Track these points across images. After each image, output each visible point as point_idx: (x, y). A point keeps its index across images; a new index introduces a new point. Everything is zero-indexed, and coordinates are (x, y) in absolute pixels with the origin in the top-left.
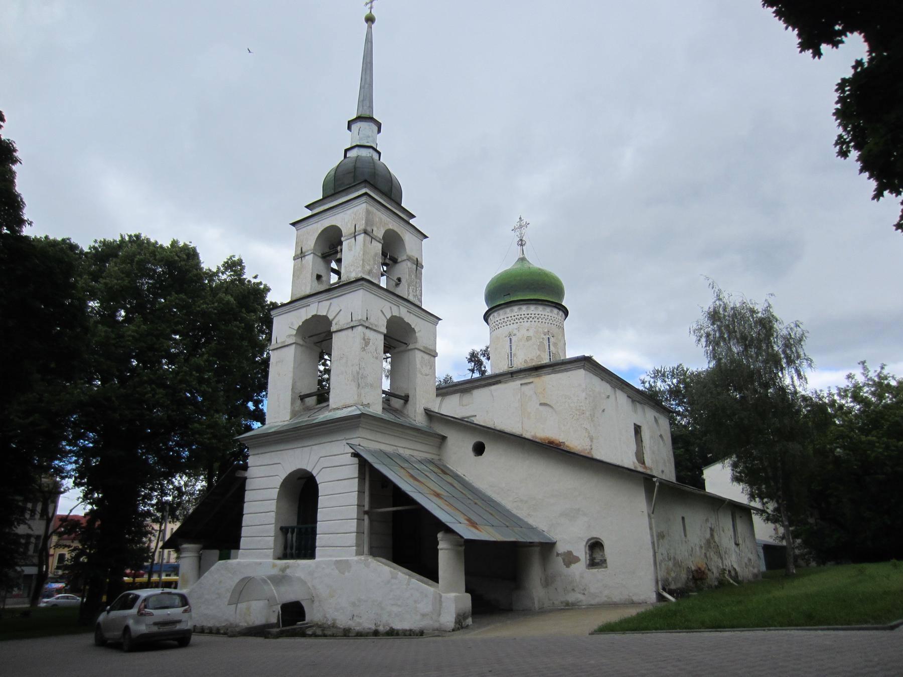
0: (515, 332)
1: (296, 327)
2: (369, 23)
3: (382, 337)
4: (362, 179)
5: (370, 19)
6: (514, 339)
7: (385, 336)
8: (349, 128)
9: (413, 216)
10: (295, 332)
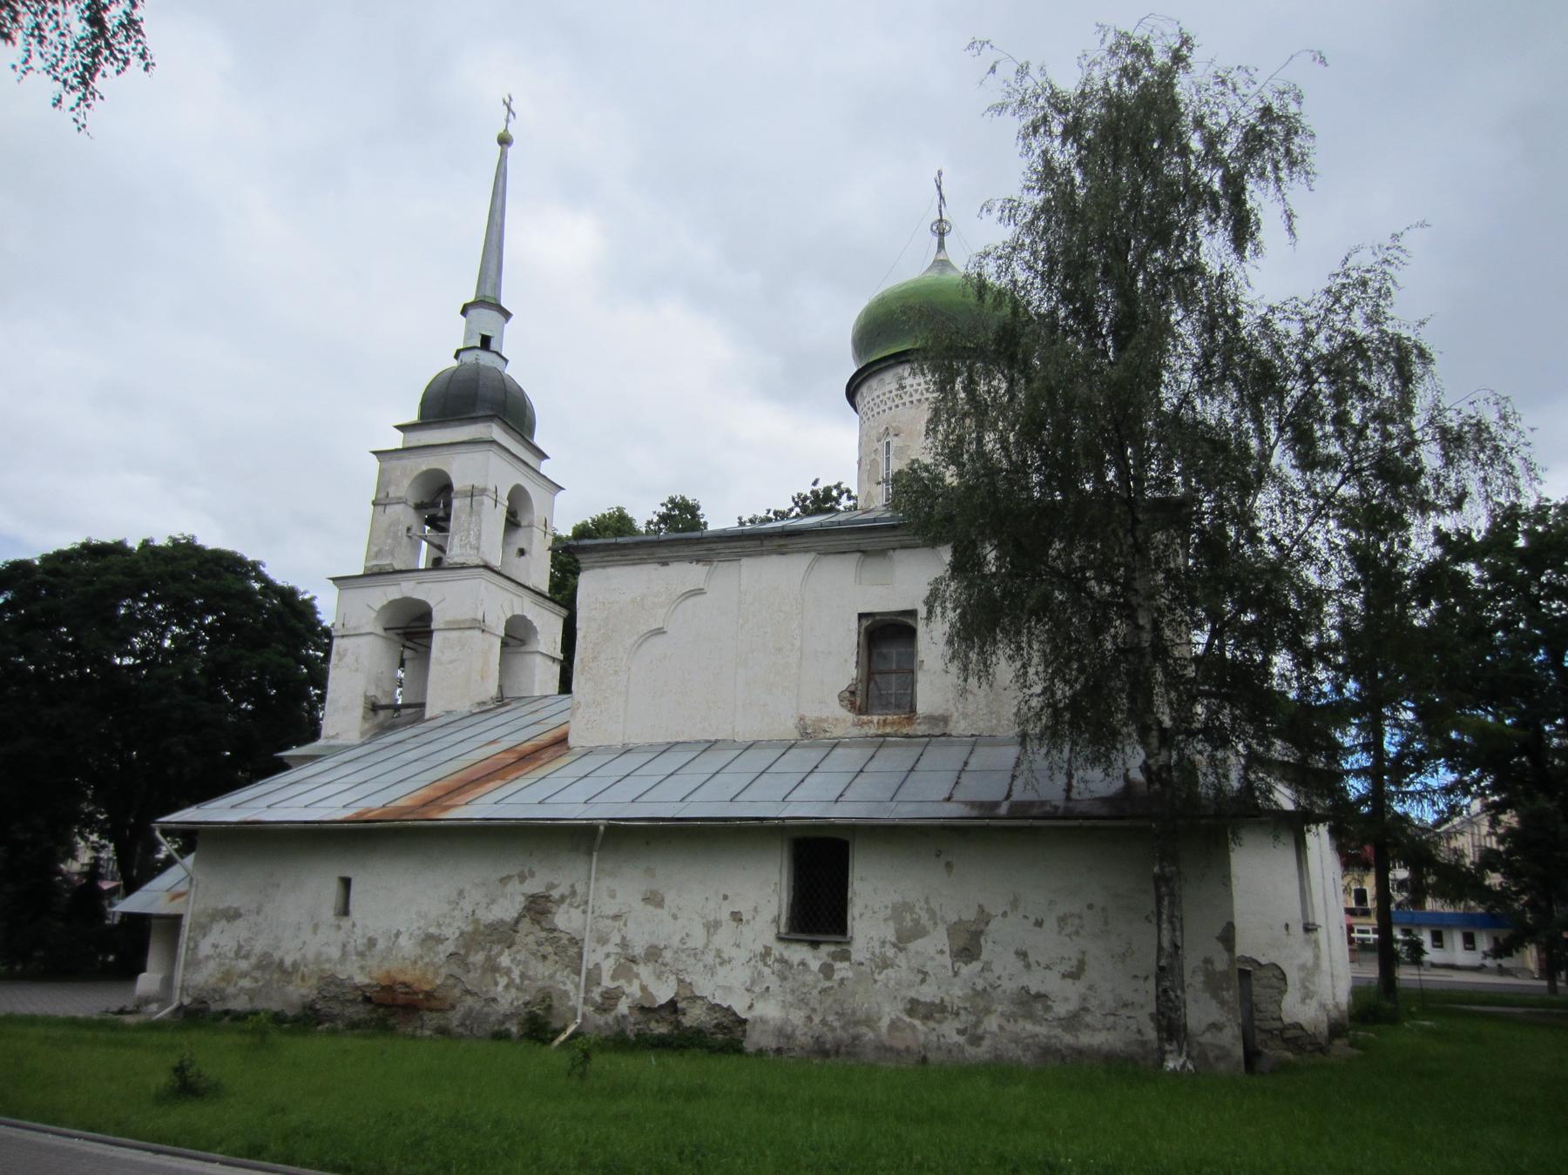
1: (378, 606)
4: (475, 399)
5: (504, 141)
8: (464, 312)
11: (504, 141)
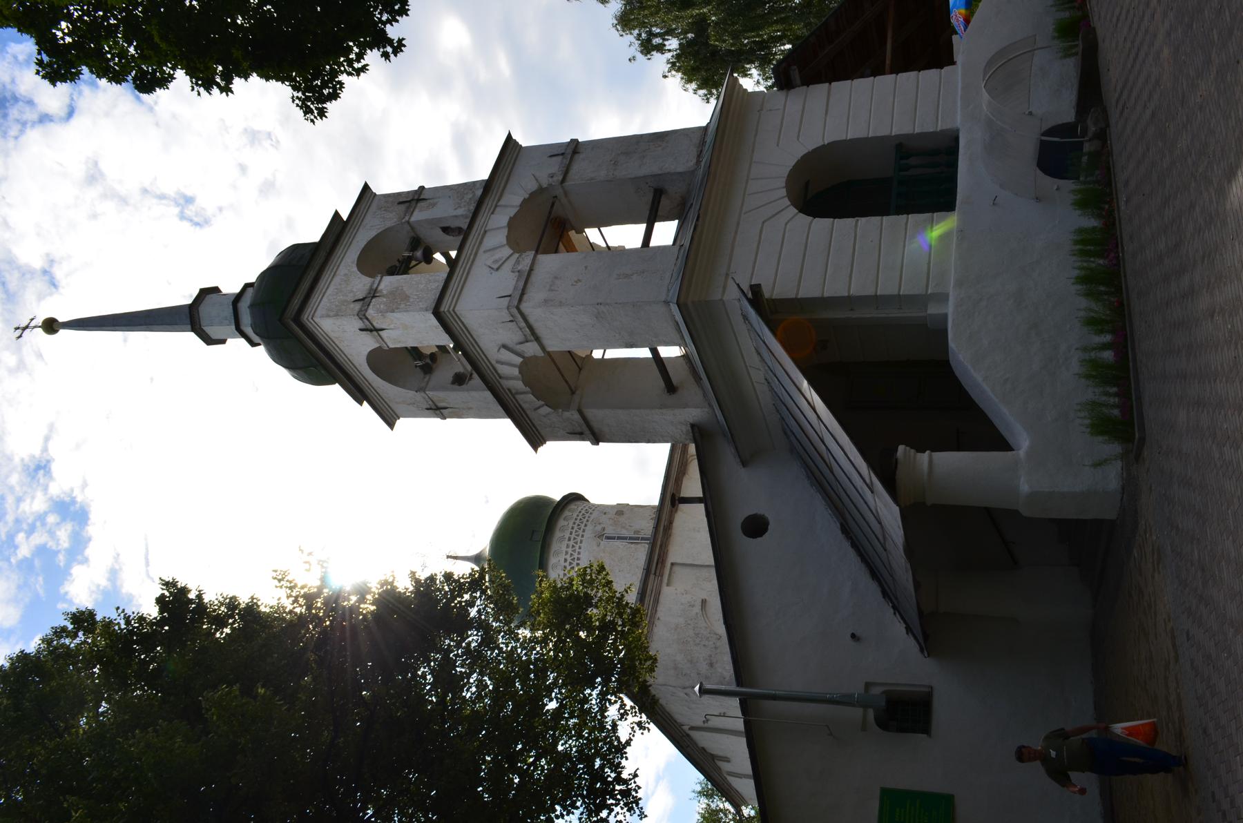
0: (599, 528)
2: (55, 326)
3: (541, 257)
6: (610, 531)
7: (537, 252)
9: (337, 215)
10: (507, 251)
11: (51, 326)
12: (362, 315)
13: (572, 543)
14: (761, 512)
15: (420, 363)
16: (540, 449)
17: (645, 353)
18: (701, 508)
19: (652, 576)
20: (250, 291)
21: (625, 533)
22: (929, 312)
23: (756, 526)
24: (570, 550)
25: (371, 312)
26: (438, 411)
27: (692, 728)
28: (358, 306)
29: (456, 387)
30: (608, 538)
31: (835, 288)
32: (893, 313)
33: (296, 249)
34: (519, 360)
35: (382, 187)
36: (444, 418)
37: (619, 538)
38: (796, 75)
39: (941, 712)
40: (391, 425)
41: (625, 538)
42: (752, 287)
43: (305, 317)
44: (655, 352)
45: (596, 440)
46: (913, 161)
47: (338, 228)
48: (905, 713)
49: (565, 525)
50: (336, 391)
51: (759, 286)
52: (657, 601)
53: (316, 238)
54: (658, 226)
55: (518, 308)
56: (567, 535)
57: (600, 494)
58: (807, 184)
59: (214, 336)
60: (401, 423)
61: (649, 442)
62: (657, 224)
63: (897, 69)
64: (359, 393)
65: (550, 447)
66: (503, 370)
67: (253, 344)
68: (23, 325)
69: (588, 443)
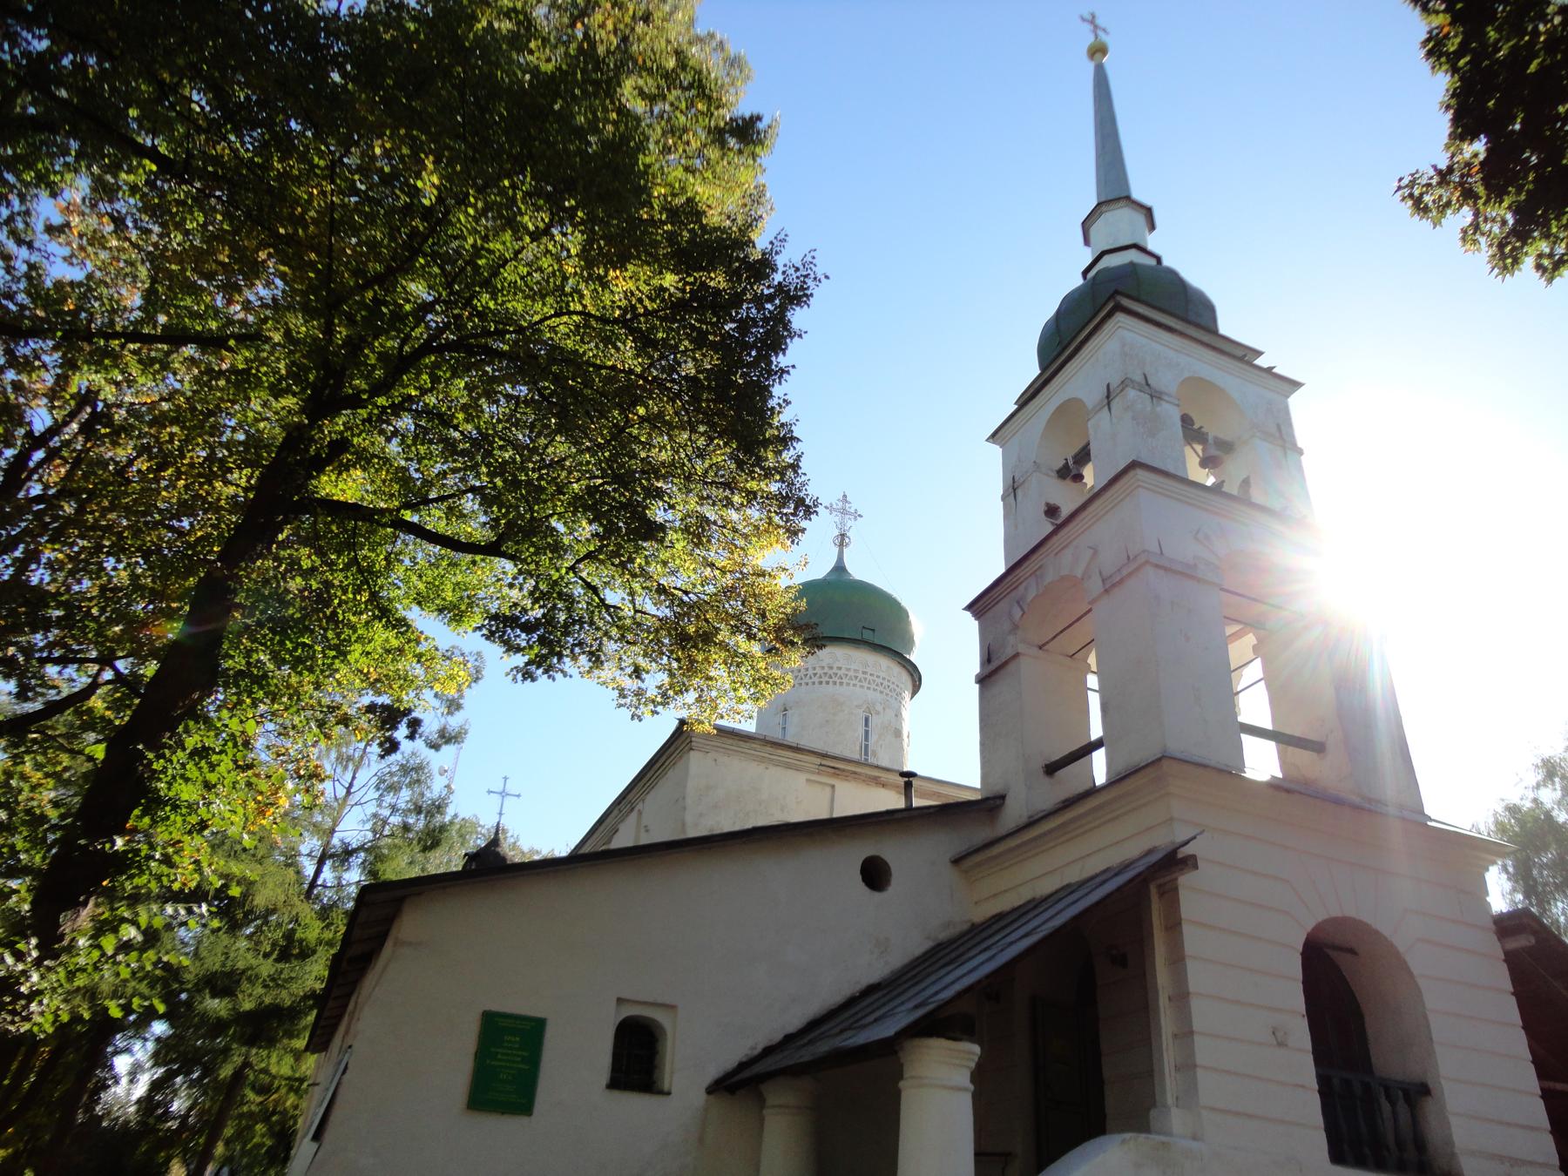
0: (879, 708)
6: (874, 721)
9: (1259, 353)
12: (1125, 383)
13: (860, 675)
14: (894, 880)
15: (1071, 462)
16: (968, 614)
17: (1096, 732)
18: (900, 803)
19: (818, 761)
20: (1153, 262)
21: (873, 738)
22: (1174, 1111)
23: (875, 875)
24: (851, 673)
25: (1131, 393)
26: (1013, 490)
27: (640, 813)
28: (1139, 378)
29: (1043, 508)
30: (867, 720)
31: (1202, 1014)
32: (1167, 1023)
33: (1209, 309)
34: (1079, 573)
35: (1297, 403)
36: (1003, 498)
37: (867, 732)
38: (1522, 942)
39: (635, 1104)
40: (994, 437)
41: (867, 739)
42: (1194, 857)
43: (1120, 318)
44: (1098, 744)
45: (982, 680)
46: (1402, 1107)
47: (1243, 355)
48: (637, 1057)
49: (882, 665)
50: (1035, 371)
51: (1196, 867)
52: (788, 766)
53: (1224, 329)
54: (1270, 747)
55: (1147, 562)
56: (869, 670)
57: (915, 714)
58: (1352, 951)
59: (1093, 231)
60: (996, 451)
61: (982, 744)
62: (1273, 744)
63: (1546, 1095)
64: (1028, 397)
65: (971, 625)
66: (1067, 556)
67: (1085, 273)
68: (1099, 22)
69: (977, 670)
